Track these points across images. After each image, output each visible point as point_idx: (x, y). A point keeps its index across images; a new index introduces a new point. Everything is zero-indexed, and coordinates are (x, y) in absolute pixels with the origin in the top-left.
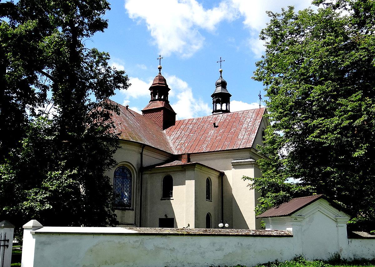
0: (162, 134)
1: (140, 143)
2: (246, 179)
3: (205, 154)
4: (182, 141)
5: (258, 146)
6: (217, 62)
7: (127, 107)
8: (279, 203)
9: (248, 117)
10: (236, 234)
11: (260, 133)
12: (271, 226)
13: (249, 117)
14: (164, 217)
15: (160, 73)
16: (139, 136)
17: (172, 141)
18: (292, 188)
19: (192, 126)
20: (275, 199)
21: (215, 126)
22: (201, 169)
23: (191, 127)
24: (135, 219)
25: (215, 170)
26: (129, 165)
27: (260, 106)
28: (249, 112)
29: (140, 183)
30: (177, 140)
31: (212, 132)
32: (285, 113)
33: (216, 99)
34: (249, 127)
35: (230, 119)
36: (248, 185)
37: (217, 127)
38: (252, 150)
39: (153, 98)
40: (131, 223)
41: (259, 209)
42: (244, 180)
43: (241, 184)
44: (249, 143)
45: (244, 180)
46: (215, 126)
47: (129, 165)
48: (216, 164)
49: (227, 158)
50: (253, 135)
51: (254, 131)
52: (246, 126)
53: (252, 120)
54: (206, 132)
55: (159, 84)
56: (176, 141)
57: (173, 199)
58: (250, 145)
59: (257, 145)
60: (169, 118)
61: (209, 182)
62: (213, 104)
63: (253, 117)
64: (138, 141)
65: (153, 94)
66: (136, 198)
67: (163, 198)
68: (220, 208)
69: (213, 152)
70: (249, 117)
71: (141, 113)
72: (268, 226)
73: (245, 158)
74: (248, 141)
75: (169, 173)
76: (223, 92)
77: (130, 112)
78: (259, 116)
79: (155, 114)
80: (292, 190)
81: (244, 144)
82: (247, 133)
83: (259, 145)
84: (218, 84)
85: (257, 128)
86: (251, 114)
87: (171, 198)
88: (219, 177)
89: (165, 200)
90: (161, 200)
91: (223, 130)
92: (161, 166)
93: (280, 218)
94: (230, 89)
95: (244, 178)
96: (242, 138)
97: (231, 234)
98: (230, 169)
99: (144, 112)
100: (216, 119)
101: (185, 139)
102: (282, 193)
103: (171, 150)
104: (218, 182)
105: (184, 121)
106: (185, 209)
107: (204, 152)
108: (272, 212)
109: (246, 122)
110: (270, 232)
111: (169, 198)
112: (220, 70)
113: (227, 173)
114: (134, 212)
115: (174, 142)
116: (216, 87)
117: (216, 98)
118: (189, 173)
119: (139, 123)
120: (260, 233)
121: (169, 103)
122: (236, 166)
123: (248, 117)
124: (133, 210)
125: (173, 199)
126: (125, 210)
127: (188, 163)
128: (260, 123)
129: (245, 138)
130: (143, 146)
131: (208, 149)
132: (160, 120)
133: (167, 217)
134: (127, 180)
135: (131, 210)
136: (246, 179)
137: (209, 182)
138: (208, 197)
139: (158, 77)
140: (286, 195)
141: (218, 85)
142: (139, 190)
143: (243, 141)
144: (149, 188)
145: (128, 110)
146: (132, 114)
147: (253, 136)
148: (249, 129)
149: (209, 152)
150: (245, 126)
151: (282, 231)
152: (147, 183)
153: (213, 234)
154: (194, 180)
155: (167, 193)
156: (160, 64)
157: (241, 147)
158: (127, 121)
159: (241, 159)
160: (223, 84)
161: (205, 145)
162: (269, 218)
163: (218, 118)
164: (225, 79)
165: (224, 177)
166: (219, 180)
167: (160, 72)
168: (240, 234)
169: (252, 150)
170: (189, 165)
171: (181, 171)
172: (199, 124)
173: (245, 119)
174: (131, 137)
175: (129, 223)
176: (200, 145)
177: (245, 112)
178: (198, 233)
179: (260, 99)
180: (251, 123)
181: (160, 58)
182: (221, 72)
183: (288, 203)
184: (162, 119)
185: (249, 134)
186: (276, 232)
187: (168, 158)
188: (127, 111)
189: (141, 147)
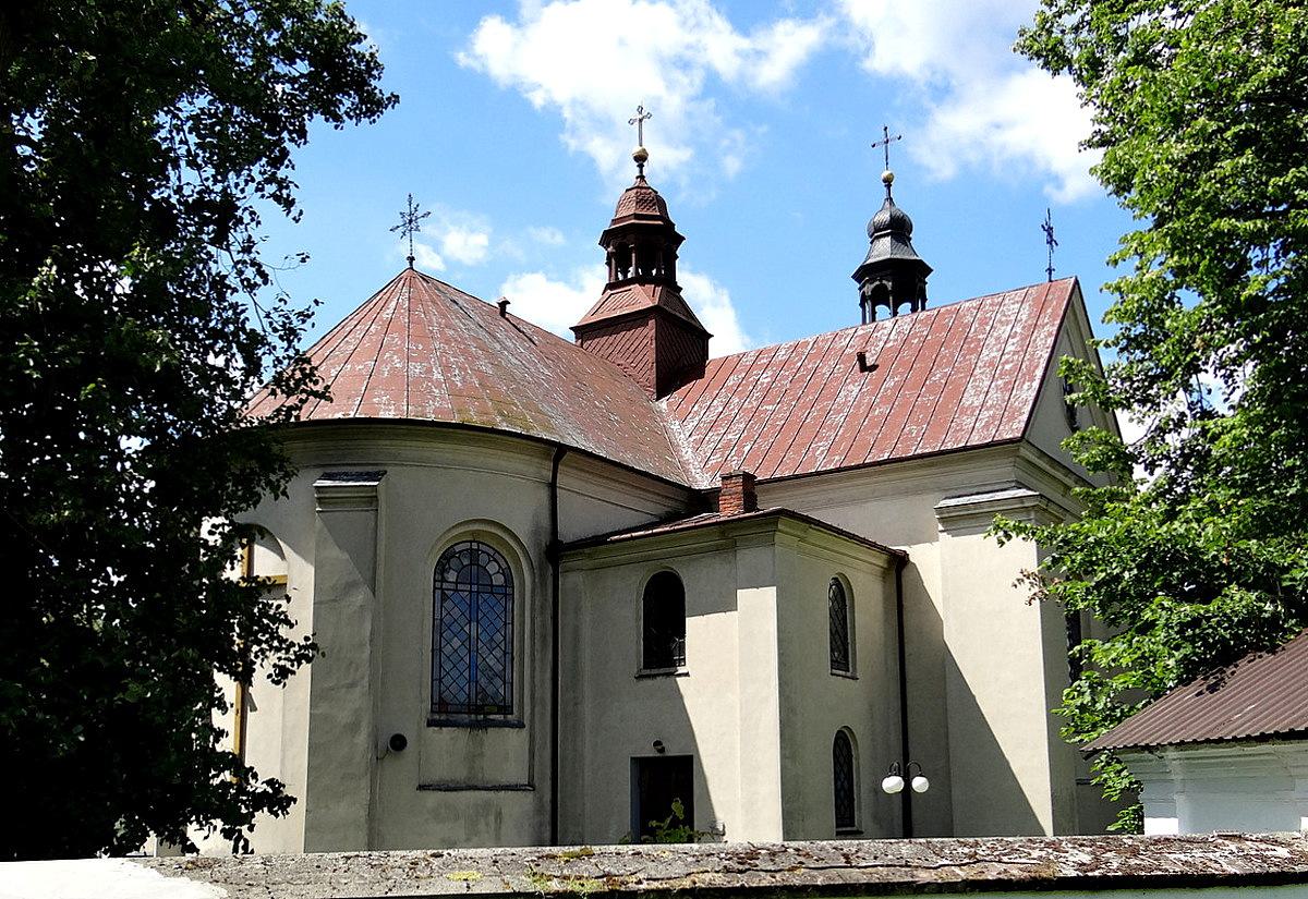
0: (652, 415)
1: (540, 440)
2: (1014, 534)
3: (822, 482)
4: (730, 437)
5: (1070, 366)
6: (874, 146)
7: (504, 304)
8: (1212, 659)
9: (1001, 322)
10: (962, 874)
11: (1053, 388)
12: (1180, 799)
13: (1004, 319)
14: (651, 753)
15: (641, 177)
16: (540, 412)
17: (691, 439)
18: (1291, 566)
19: (770, 373)
20: (1192, 640)
21: (864, 368)
22: (802, 539)
23: (765, 380)
24: (531, 767)
25: (863, 541)
26: (500, 533)
27: (1050, 270)
28: (1006, 301)
29: (549, 612)
30: (710, 434)
31: (854, 388)
32: (1228, 135)
33: (873, 286)
34: (1007, 356)
35: (925, 333)
36: (1021, 576)
37: (874, 368)
38: (1025, 452)
39: (617, 275)
40: (513, 781)
41: (1094, 702)
42: (1002, 543)
43: (987, 600)
44: (1012, 418)
45: (1002, 543)
46: (864, 368)
47: (500, 533)
48: (872, 516)
49: (918, 491)
50: (1025, 387)
51: (1028, 371)
52: (996, 354)
53: (1018, 329)
54: (828, 391)
55: (637, 216)
56: (707, 438)
57: (687, 674)
58: (1013, 430)
59: (1064, 358)
60: (681, 351)
61: (841, 595)
62: (862, 305)
63: (1024, 317)
64: (533, 433)
65: (618, 260)
66: (533, 677)
67: (648, 672)
68: (897, 704)
69: (858, 467)
70: (1004, 319)
71: (571, 337)
72: (1165, 801)
73: (997, 487)
74: (1007, 411)
75: (665, 563)
76: (898, 256)
77: (516, 327)
78: (1049, 310)
79: (624, 337)
80: (1293, 579)
81: (987, 426)
82: (1000, 382)
83: (1071, 360)
84: (877, 230)
85: (1042, 360)
86: (1012, 306)
87: (681, 670)
88: (885, 573)
89: (655, 676)
90: (640, 677)
91: (896, 379)
92: (634, 534)
93: (1248, 750)
94: (922, 246)
95: (1001, 533)
96: (976, 403)
97: (924, 877)
98: (932, 539)
99: (582, 332)
100: (868, 339)
101: (742, 426)
102: (1238, 599)
103: (686, 471)
104: (884, 592)
105: (740, 357)
106: (738, 715)
107: (818, 473)
108: (1183, 712)
109: (991, 341)
110: (1198, 853)
111: (672, 670)
112: (886, 174)
113: (918, 554)
114: (525, 733)
115: (696, 442)
116: (872, 243)
117: (871, 281)
118: (749, 557)
119: (548, 367)
120: (1133, 862)
121: (681, 294)
122: (955, 521)
123: (1001, 322)
124: (520, 725)
125: (687, 674)
126: (487, 725)
127: (747, 514)
128: (1053, 338)
129: (990, 402)
130: (558, 453)
131: (837, 458)
132: (645, 360)
133: (662, 750)
134: (492, 601)
135: (512, 726)
136: (1009, 537)
137: (841, 595)
138: (842, 656)
139: (635, 191)
140: (1261, 610)
141: (877, 232)
142: (544, 637)
143: (985, 414)
144: (587, 632)
145: (507, 319)
146: (523, 333)
147: (1028, 392)
148: (1007, 367)
149: (838, 470)
150: (992, 355)
151: (1276, 842)
152: (577, 610)
153: (797, 882)
154: (775, 588)
155: (663, 648)
156: (641, 139)
157: (975, 441)
158: (492, 357)
159: (975, 490)
160: (899, 228)
161: (823, 446)
162: (1171, 754)
163: (875, 335)
164: (904, 206)
165: (905, 572)
166: (884, 587)
167: (641, 172)
168: (991, 875)
169: (1025, 452)
170: (746, 522)
171: (718, 549)
172: (799, 364)
173: (988, 328)
174: (502, 414)
175: (504, 781)
176: (804, 444)
177: (989, 302)
178: (687, 884)
179: (1050, 242)
180: (1015, 340)
181: (641, 116)
182: (888, 182)
183: (1282, 656)
184: (651, 356)
185: (1010, 388)
186: (1233, 847)
187: (670, 503)
188: (503, 322)
189: (546, 456)
